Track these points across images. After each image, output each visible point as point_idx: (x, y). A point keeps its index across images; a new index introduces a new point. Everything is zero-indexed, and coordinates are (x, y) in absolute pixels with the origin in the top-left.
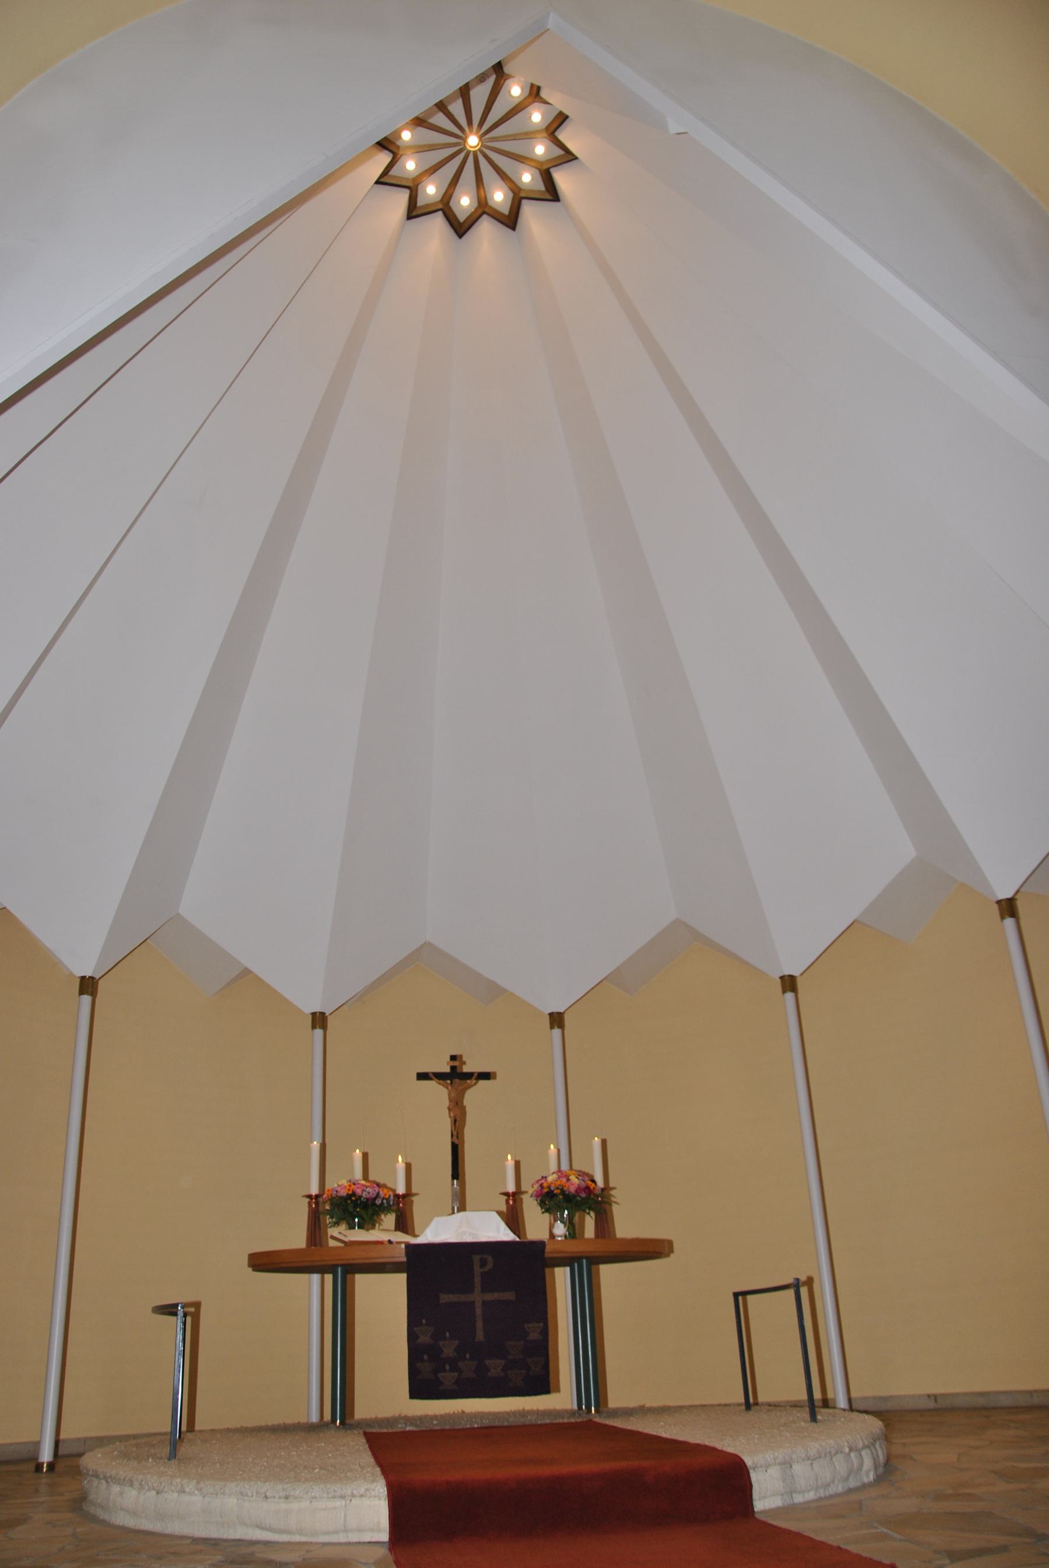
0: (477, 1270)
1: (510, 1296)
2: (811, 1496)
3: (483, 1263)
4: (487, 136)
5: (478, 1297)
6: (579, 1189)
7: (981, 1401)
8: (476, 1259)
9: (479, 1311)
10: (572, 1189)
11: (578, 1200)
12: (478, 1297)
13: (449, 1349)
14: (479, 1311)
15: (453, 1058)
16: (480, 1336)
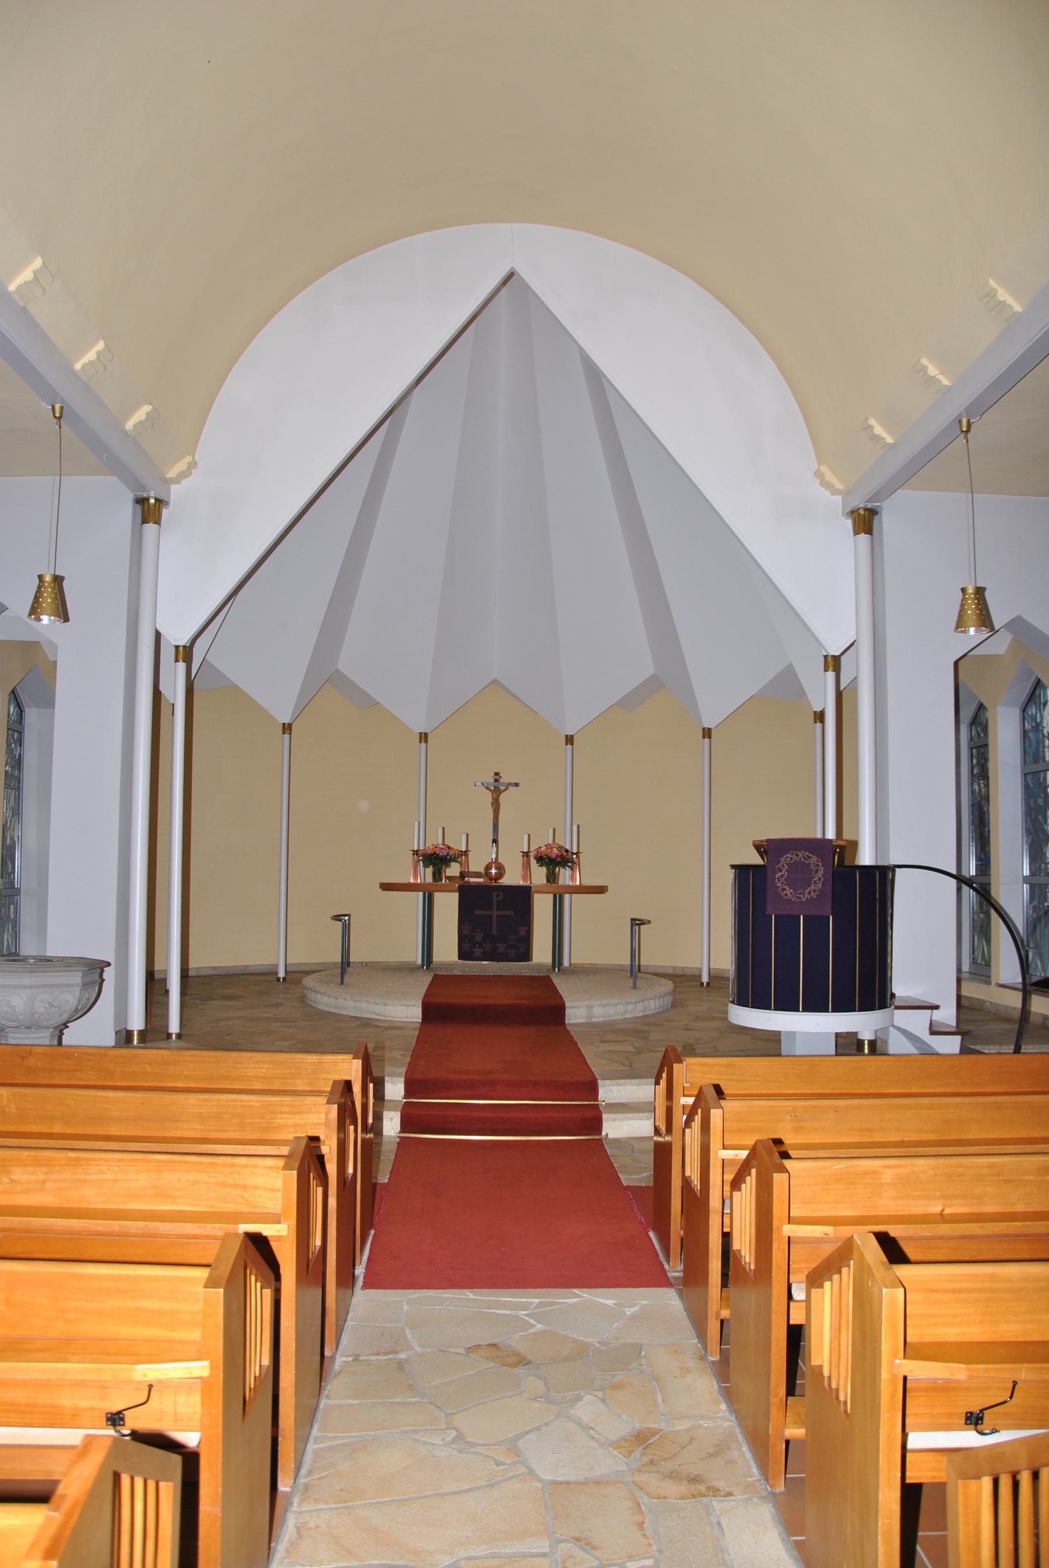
0: (495, 899)
1: (510, 913)
2: (601, 1019)
3: (498, 896)
4: (303, 1471)
5: (495, 913)
6: (557, 856)
7: (224, 972)
8: (495, 894)
9: (494, 919)
10: (554, 856)
11: (556, 860)
12: (495, 913)
13: (478, 937)
14: (494, 919)
15: (496, 774)
16: (494, 932)
